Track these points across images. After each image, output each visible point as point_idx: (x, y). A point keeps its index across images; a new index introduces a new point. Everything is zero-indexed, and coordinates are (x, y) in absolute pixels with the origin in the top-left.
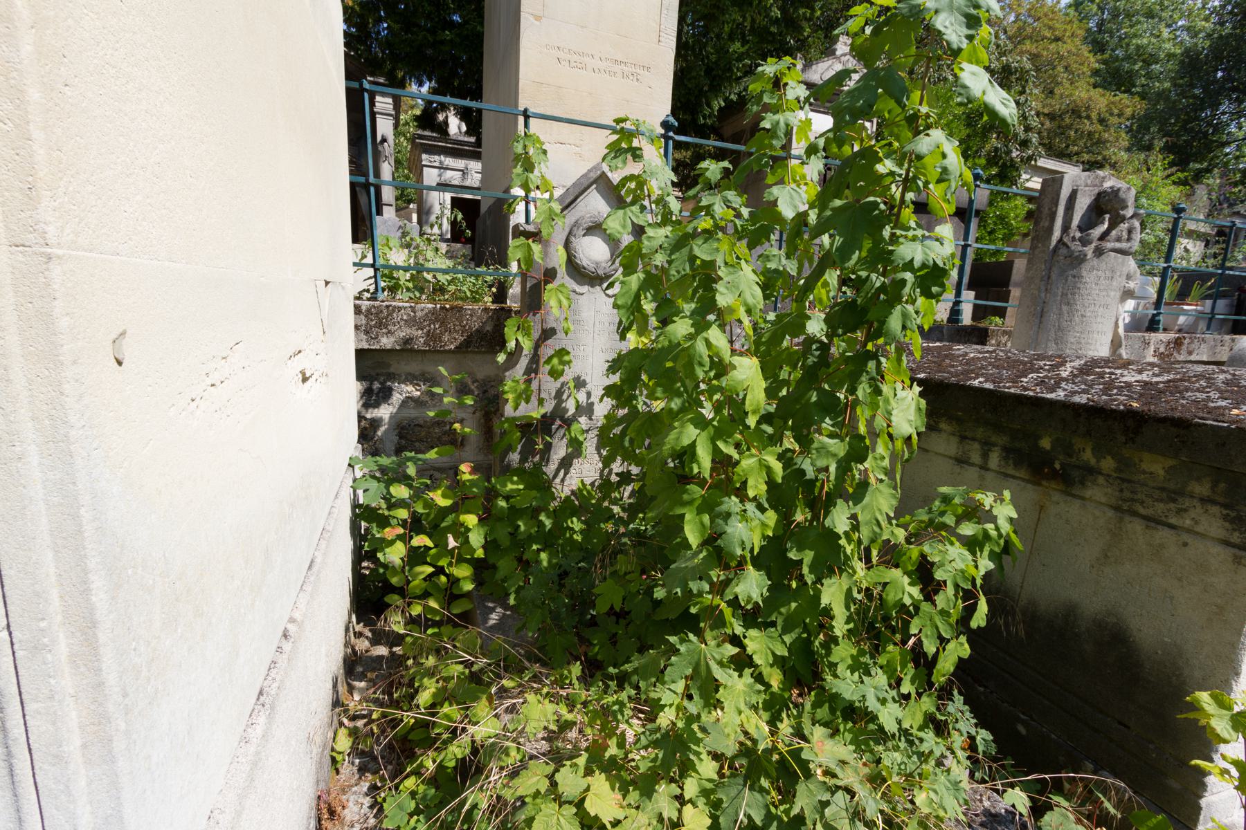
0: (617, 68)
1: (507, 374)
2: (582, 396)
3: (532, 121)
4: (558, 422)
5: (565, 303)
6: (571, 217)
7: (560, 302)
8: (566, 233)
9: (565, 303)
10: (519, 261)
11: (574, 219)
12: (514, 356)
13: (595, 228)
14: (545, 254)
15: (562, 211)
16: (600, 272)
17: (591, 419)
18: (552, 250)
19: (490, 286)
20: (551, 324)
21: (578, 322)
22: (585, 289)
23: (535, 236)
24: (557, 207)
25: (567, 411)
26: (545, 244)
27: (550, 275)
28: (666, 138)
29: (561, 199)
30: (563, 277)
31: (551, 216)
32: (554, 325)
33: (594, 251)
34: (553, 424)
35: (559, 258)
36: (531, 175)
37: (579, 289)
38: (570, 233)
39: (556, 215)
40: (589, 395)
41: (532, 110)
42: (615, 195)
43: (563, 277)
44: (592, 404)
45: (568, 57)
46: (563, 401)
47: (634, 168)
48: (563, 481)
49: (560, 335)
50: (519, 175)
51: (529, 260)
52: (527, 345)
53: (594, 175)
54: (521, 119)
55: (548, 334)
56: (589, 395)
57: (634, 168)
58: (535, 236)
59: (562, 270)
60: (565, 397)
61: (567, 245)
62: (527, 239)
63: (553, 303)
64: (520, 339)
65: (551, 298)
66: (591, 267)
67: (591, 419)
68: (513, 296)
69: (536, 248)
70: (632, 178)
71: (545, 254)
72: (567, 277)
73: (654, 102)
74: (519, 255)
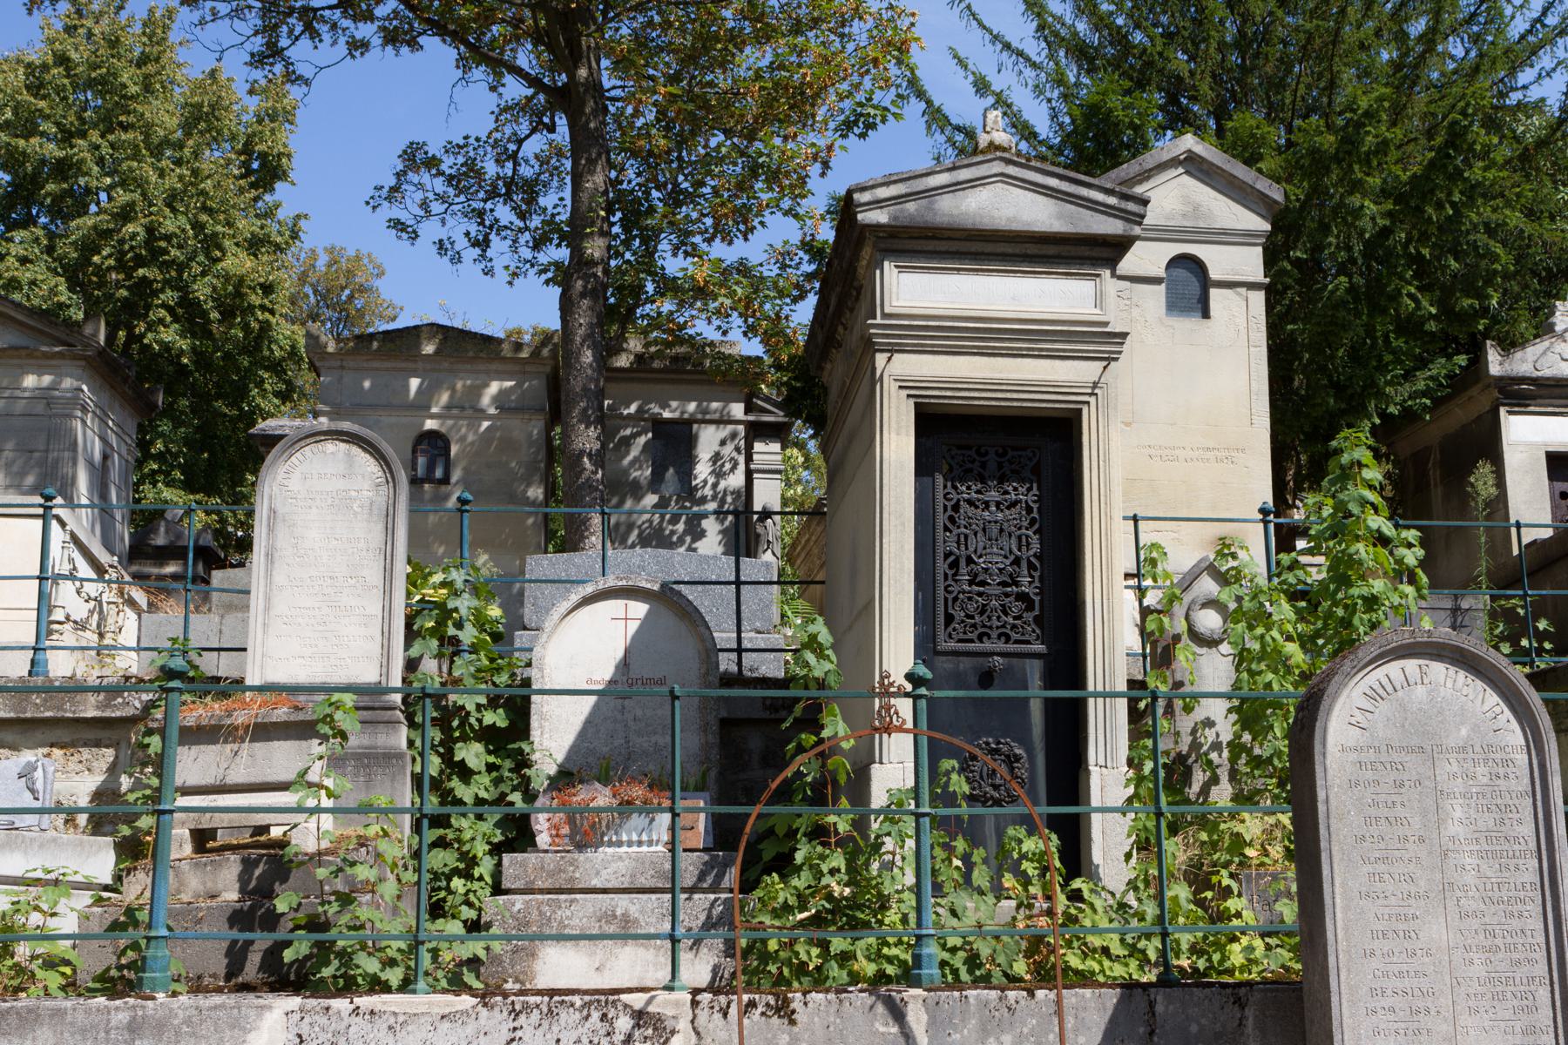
0: (1210, 455)
3: (1523, 530)
6: (1187, 598)
13: (1211, 603)
20: (1178, 677)
21: (1200, 677)
22: (1204, 650)
27: (1177, 638)
28: (1266, 523)
33: (1209, 621)
35: (1181, 626)
41: (1140, 515)
42: (1223, 579)
45: (1159, 452)
47: (1232, 563)
54: (1514, 530)
57: (1232, 563)
59: (1185, 637)
61: (1187, 617)
66: (1208, 633)
69: (1166, 620)
70: (1233, 568)
73: (1255, 481)
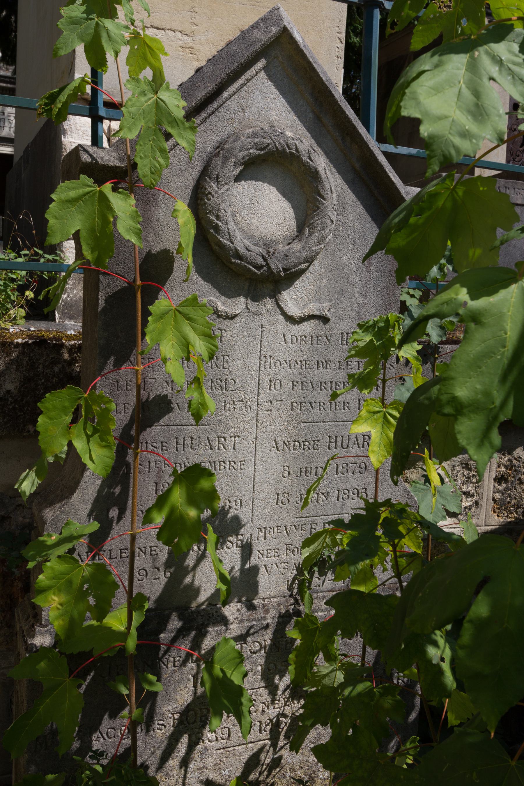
1: (49, 514)
2: (230, 557)
4: (175, 623)
5: (199, 346)
7: (186, 345)
8: (194, 173)
9: (199, 346)
10: (76, 237)
11: (213, 140)
12: (63, 478)
14: (145, 221)
15: (192, 113)
16: (276, 265)
17: (251, 607)
18: (161, 213)
19: (21, 290)
20: (157, 388)
22: (238, 305)
23: (122, 176)
24: (177, 105)
25: (197, 592)
26: (148, 199)
27: (157, 268)
29: (185, 89)
30: (186, 283)
31: (161, 127)
32: (166, 391)
34: (162, 628)
35: (179, 226)
36: (108, 23)
37: (224, 305)
38: (205, 172)
39: (174, 122)
40: (247, 550)
43: (186, 283)
44: (255, 570)
46: (186, 571)
48: (185, 763)
49: (180, 415)
50: (74, 22)
51: (102, 236)
52: (96, 459)
53: (262, 37)
55: (151, 410)
56: (247, 550)
58: (122, 176)
60: (190, 561)
61: (198, 200)
62: (100, 182)
63: (168, 348)
64: (79, 445)
65: (167, 350)
66: (240, 243)
67: (251, 607)
68: (68, 305)
69: (123, 205)
71: (145, 221)
72: (195, 277)
74: (77, 224)
